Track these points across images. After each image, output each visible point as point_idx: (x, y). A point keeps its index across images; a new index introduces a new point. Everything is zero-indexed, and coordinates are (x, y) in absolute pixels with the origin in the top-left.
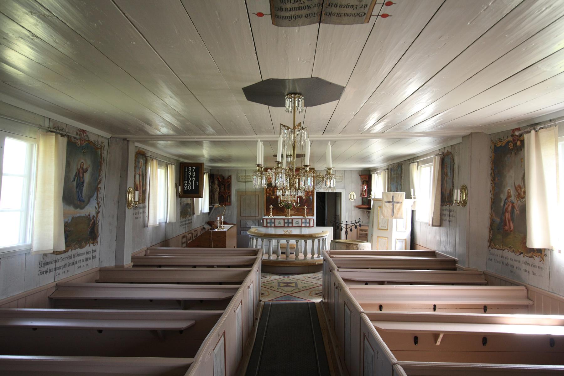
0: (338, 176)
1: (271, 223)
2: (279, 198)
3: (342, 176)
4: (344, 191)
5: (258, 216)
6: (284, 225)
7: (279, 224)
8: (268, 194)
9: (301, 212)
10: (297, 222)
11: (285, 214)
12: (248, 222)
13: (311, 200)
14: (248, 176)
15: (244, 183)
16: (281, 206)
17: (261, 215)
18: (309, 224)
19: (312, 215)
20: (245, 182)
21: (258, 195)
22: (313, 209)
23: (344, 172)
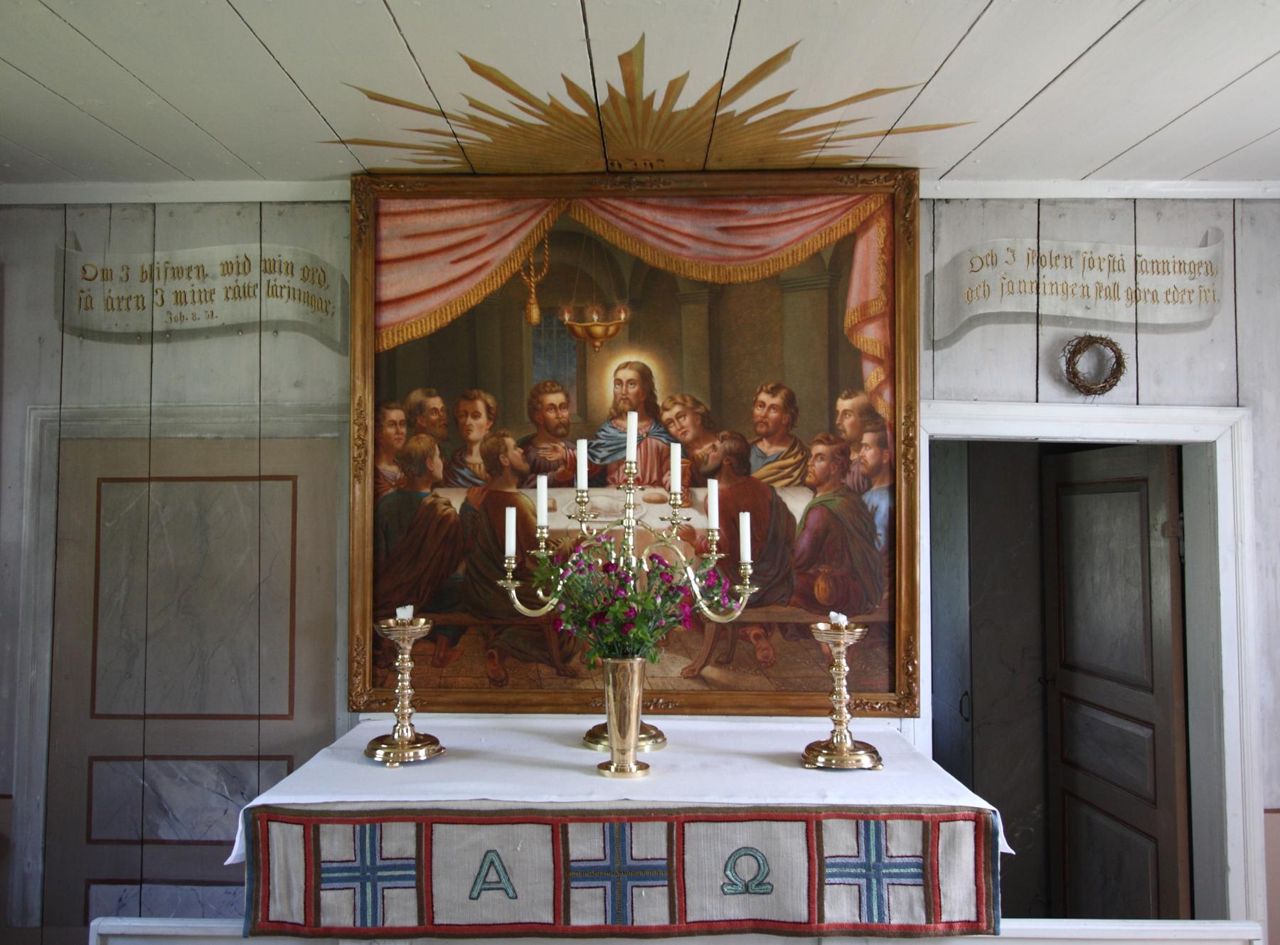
0: (1160, 267)
2: (511, 514)
3: (1211, 269)
4: (1245, 430)
5: (290, 716)
6: (561, 903)
7: (480, 886)
8: (391, 470)
9: (763, 667)
10: (747, 868)
11: (586, 685)
12: (173, 776)
13: (881, 531)
14: (177, 272)
15: (142, 350)
16: (535, 603)
17: (324, 704)
18: (917, 893)
19: (891, 698)
20: (150, 337)
21: (293, 479)
22: (903, 627)
23: (1226, 225)
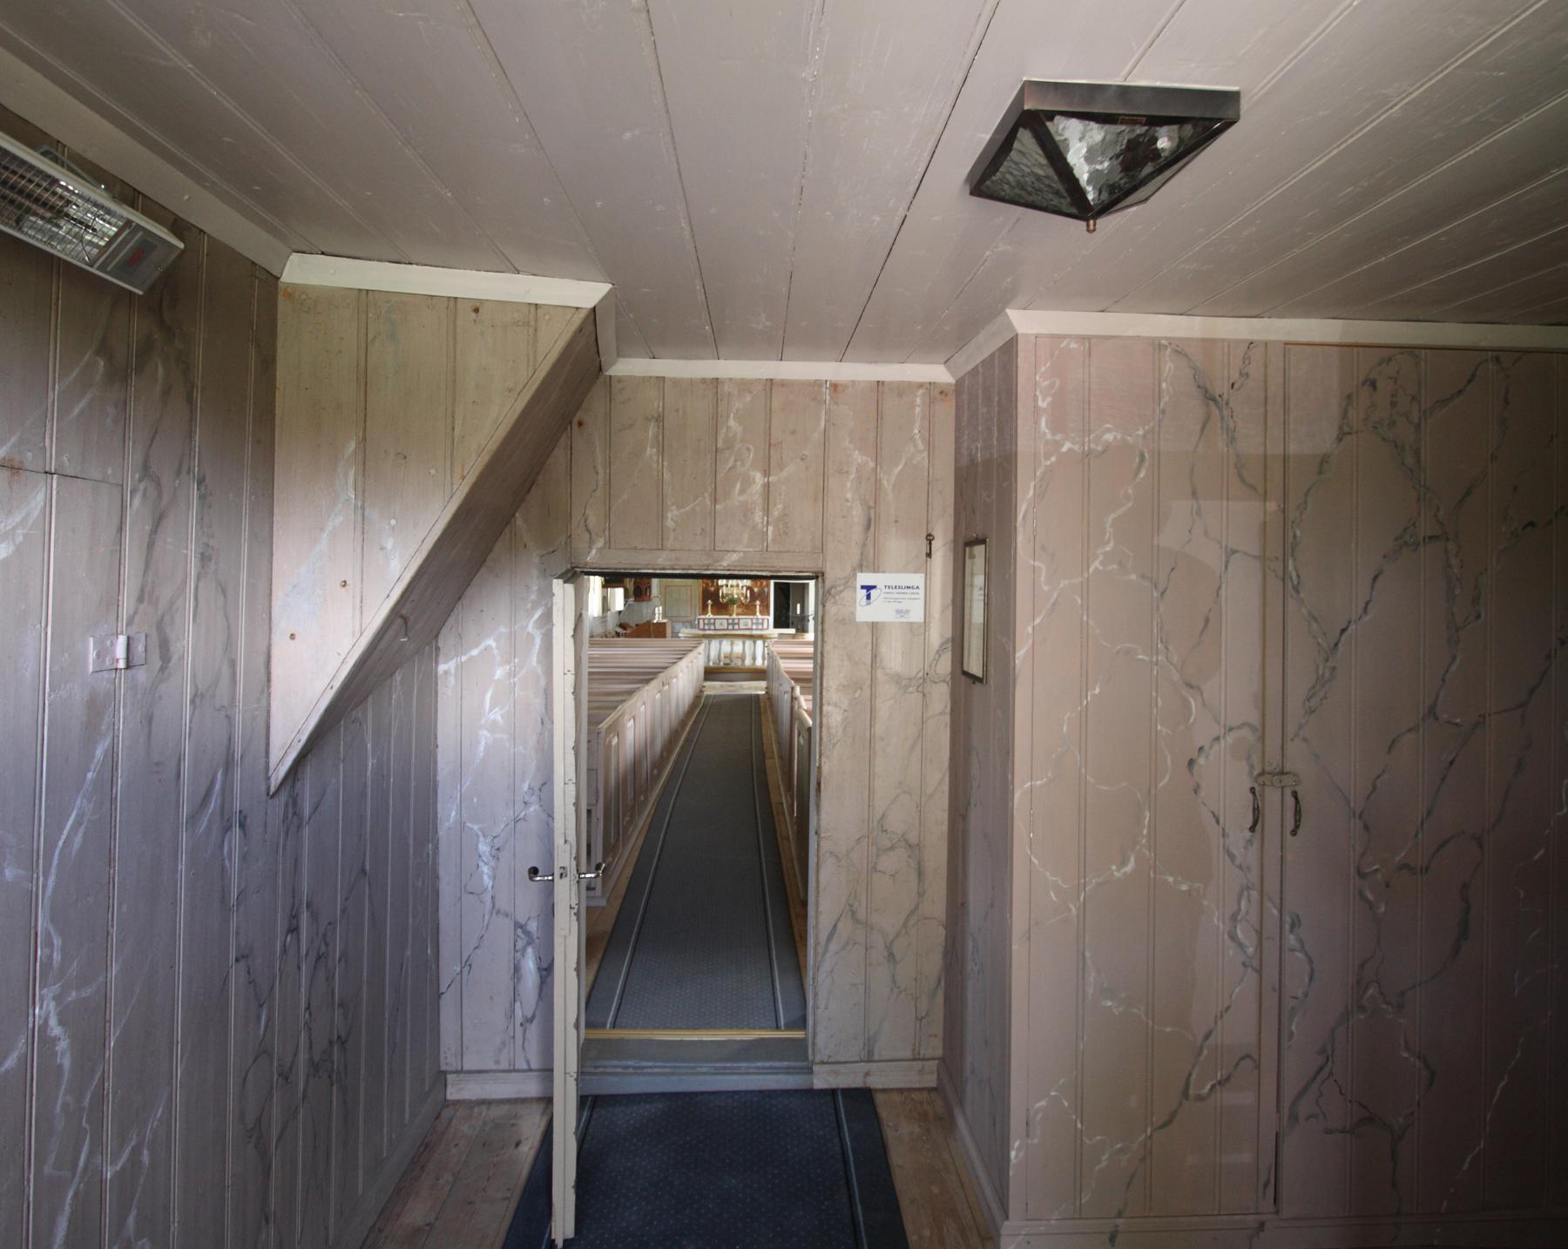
1: (709, 624)
